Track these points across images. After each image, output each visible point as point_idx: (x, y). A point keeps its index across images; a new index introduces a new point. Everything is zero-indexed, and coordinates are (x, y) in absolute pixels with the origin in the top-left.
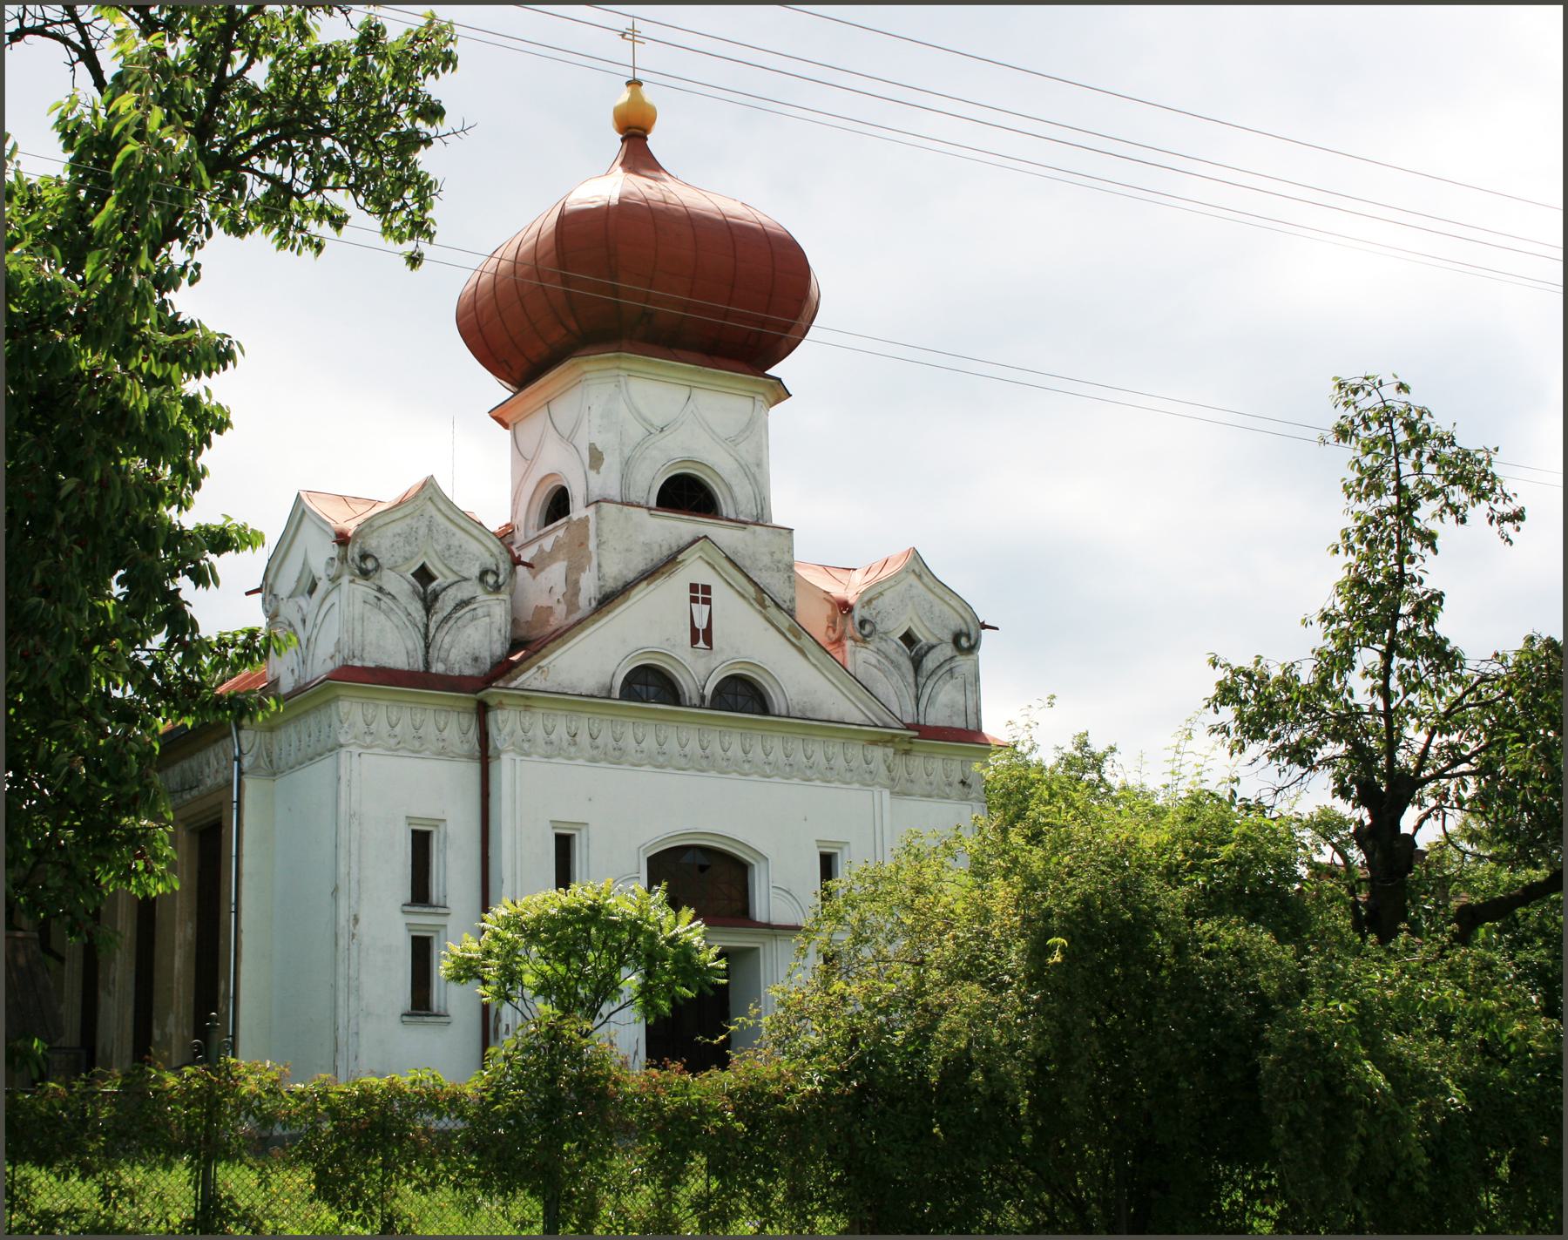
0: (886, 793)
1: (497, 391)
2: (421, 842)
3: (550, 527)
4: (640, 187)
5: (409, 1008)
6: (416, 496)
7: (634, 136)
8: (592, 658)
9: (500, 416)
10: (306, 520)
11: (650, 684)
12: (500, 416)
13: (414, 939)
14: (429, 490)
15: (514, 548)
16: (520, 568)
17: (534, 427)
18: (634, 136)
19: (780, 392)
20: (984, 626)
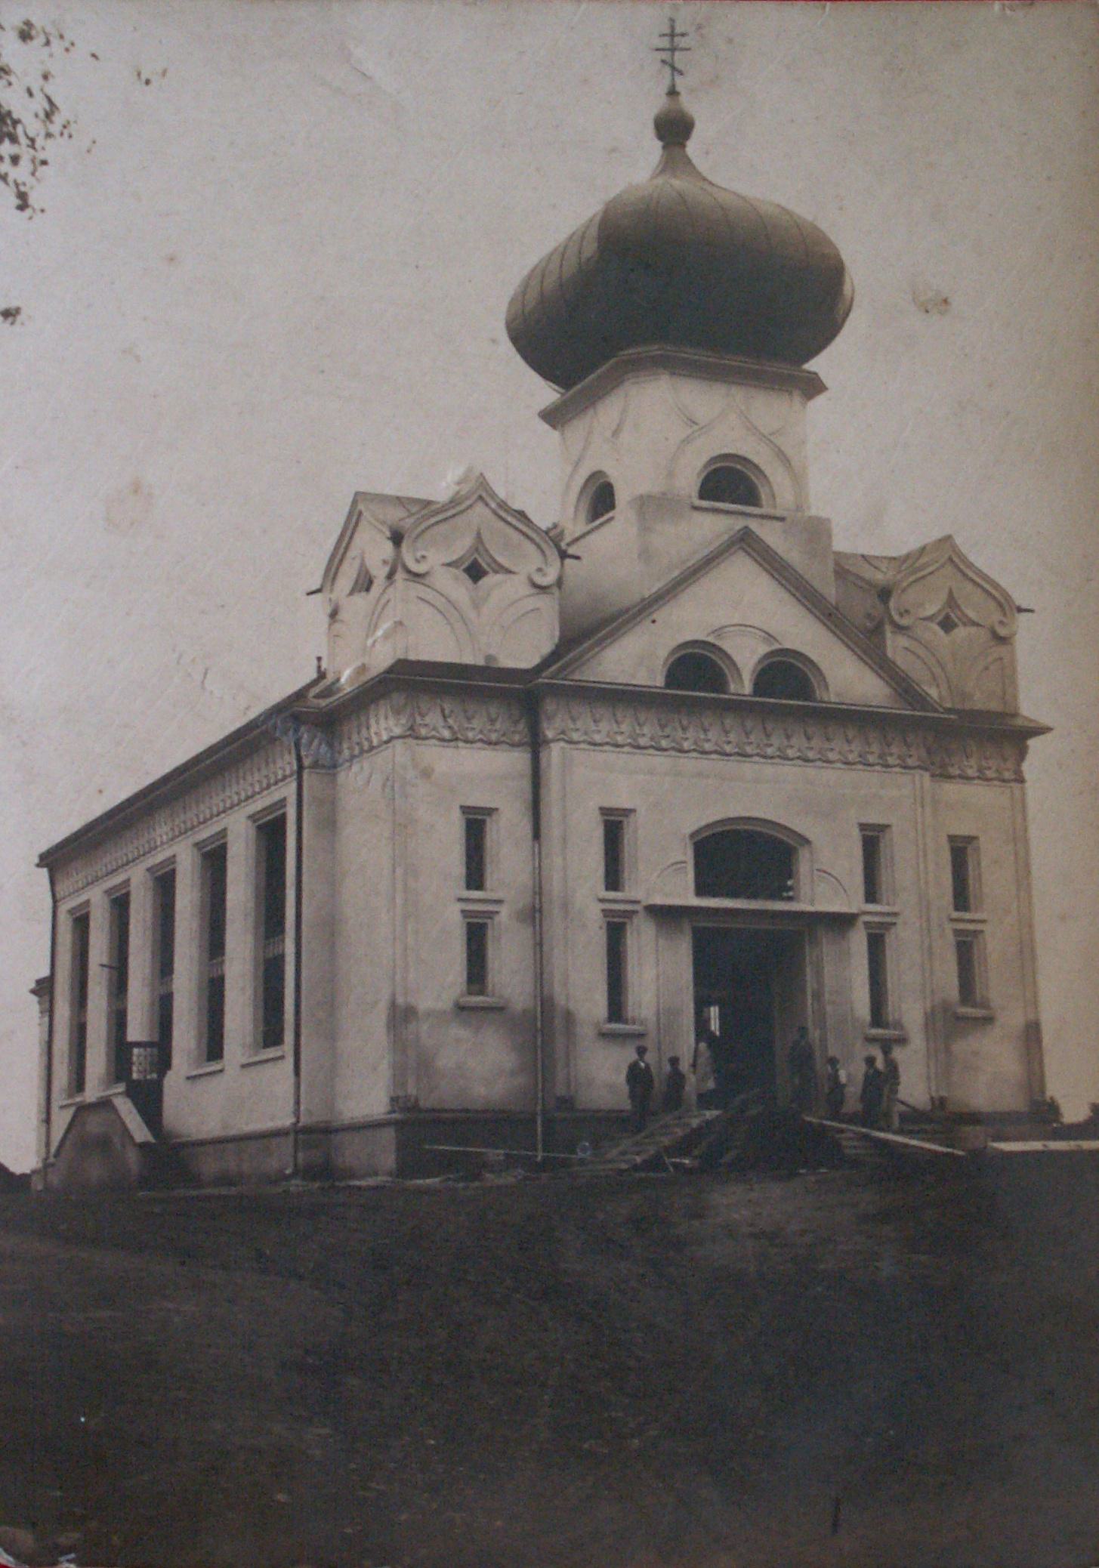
0: (927, 776)
1: (547, 394)
2: (476, 825)
3: (598, 522)
4: (678, 183)
5: (464, 987)
6: (264, 722)
7: (674, 129)
8: (634, 659)
9: (553, 417)
10: (363, 524)
11: (696, 670)
12: (553, 417)
13: (470, 925)
14: (33, 992)
15: (563, 545)
16: (568, 561)
17: (578, 428)
18: (674, 129)
19: (813, 387)
20: (1020, 610)
